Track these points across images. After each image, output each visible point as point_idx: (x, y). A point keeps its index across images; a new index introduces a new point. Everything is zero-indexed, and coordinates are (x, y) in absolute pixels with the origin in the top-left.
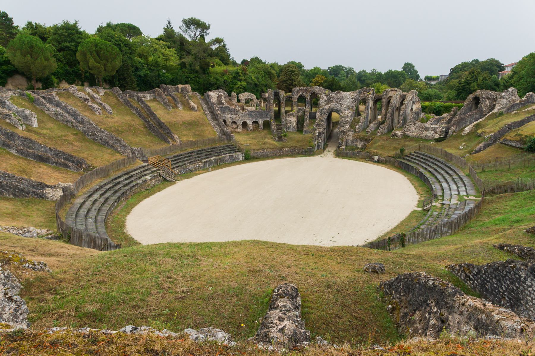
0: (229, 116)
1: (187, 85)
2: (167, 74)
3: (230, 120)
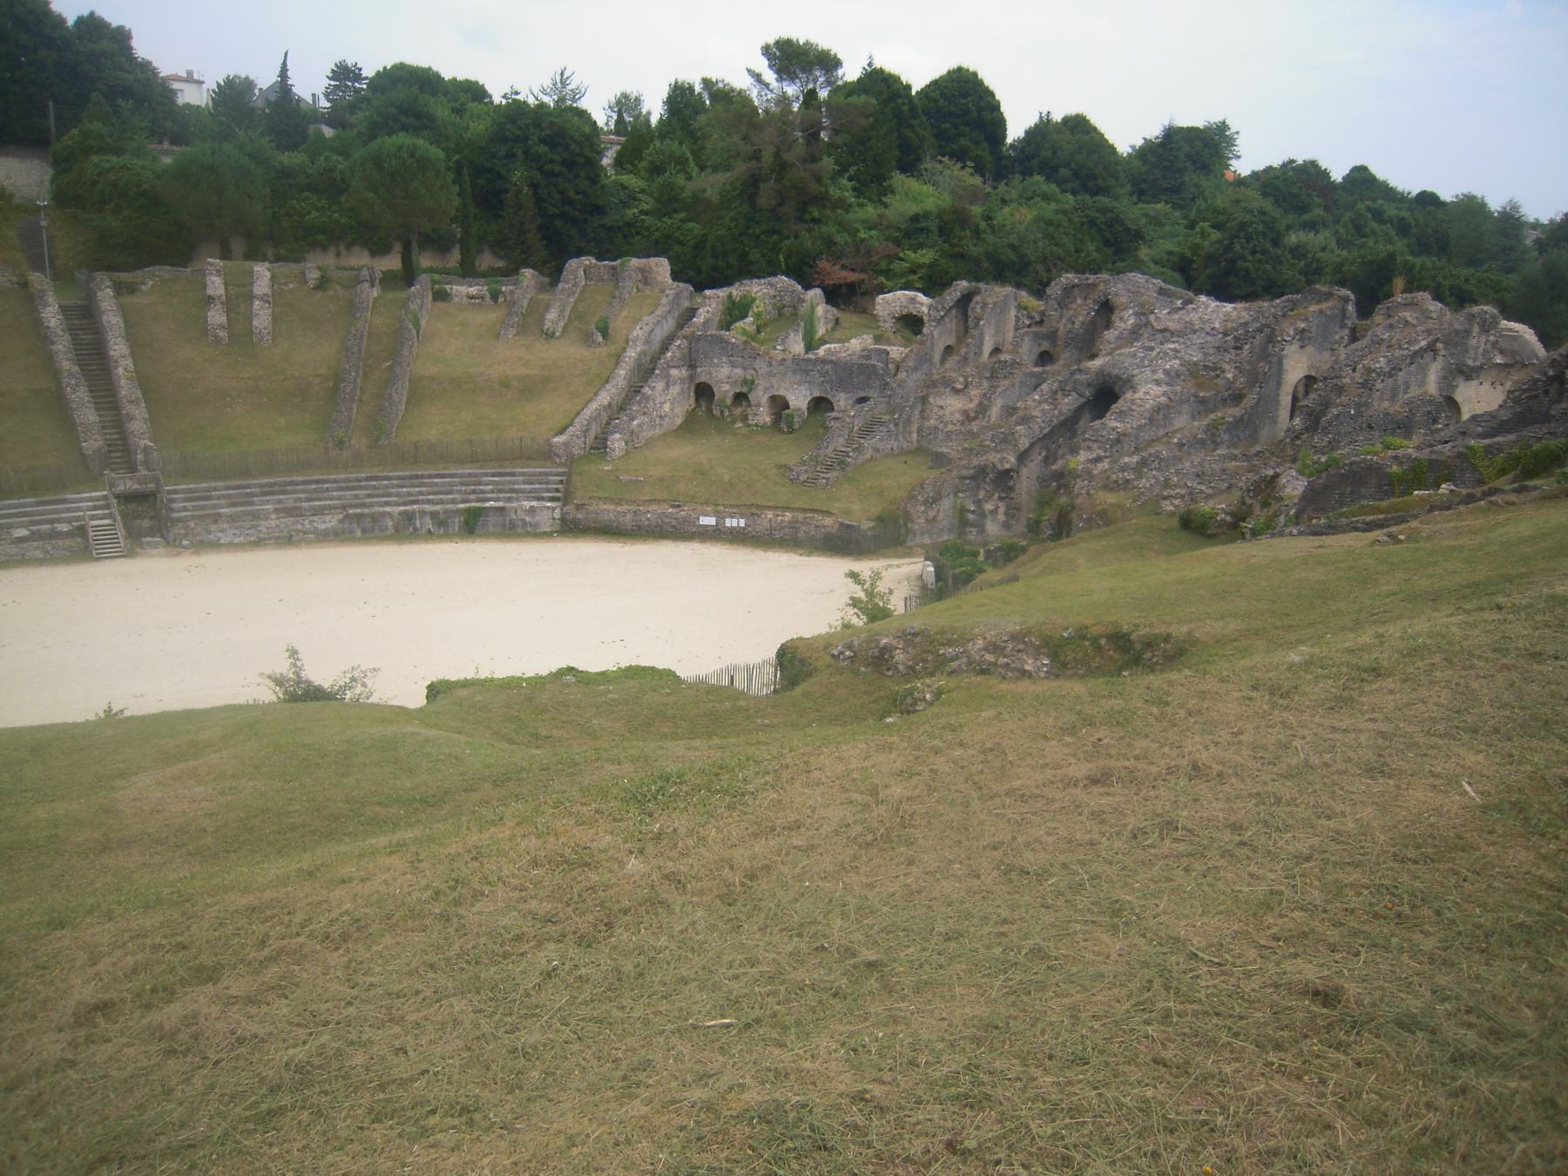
0: (725, 371)
1: (653, 261)
2: (691, 225)
3: (727, 387)
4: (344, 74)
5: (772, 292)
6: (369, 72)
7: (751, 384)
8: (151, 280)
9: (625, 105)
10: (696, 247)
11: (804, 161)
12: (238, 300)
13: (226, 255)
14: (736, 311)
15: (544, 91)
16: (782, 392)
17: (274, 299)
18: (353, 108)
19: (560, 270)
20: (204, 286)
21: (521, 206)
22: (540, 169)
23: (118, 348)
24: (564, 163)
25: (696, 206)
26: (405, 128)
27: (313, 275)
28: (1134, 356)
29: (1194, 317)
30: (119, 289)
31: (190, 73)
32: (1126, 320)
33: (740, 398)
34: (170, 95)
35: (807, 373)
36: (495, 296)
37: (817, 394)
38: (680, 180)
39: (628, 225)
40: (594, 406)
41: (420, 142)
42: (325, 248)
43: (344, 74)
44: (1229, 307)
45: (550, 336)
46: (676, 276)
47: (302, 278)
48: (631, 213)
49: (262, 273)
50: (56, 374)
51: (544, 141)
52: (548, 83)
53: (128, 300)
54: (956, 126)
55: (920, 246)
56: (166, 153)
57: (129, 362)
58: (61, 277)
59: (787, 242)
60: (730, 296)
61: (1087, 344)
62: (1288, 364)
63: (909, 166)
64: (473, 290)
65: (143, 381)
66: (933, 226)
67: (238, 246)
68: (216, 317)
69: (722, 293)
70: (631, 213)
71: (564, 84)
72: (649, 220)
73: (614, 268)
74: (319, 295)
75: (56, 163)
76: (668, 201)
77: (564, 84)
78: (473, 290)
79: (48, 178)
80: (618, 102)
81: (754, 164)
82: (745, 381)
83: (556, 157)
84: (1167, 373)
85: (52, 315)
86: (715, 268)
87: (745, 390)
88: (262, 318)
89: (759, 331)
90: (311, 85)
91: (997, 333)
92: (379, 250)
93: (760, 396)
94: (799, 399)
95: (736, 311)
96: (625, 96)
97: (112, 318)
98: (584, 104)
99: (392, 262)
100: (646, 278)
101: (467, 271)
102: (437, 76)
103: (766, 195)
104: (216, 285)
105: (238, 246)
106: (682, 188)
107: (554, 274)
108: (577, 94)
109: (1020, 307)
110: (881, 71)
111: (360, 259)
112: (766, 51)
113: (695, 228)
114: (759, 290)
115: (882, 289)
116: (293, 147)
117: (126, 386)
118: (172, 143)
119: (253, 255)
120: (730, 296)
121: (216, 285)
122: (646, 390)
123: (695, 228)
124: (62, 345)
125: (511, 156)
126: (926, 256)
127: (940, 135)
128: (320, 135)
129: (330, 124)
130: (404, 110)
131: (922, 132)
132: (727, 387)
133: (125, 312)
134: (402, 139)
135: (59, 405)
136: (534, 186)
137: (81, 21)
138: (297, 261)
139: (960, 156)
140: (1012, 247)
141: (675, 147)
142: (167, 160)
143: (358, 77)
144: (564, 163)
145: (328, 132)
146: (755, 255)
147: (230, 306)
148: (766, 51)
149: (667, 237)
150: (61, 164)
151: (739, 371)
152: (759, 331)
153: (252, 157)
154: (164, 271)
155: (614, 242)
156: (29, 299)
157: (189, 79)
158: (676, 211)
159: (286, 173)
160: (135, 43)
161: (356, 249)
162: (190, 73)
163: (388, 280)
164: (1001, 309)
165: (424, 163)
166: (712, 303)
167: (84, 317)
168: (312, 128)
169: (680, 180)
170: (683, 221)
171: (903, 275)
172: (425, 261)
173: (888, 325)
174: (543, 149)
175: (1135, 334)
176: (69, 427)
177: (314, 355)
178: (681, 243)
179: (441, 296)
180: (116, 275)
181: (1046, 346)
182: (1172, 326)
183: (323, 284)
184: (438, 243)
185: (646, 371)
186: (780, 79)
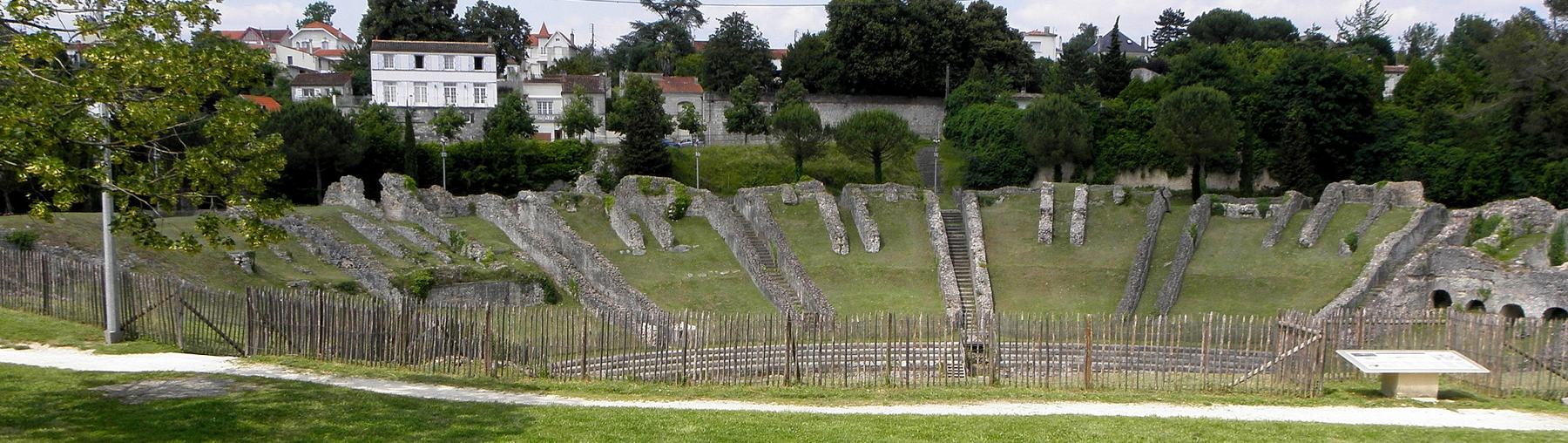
0: (1462, 281)
3: (1464, 295)
5: (1521, 212)
6: (1191, 16)
7: (1487, 293)
8: (1005, 199)
9: (1417, 35)
12: (1059, 214)
14: (1479, 228)
15: (1348, 22)
17: (1086, 214)
19: (1320, 192)
21: (1295, 137)
22: (1316, 106)
23: (976, 244)
24: (1338, 100)
25: (1467, 133)
26: (1204, 77)
27: (1119, 194)
30: (980, 201)
31: (1047, 29)
33: (1476, 305)
34: (1028, 51)
35: (1544, 285)
36: (1263, 213)
37: (1553, 305)
38: (1449, 109)
39: (1396, 150)
40: (1333, 305)
41: (1211, 89)
42: (1133, 171)
45: (1306, 247)
46: (1427, 197)
47: (1110, 195)
48: (1398, 140)
49: (1081, 191)
50: (935, 260)
52: (1352, 14)
53: (987, 210)
57: (983, 254)
59: (1552, 164)
60: (1480, 215)
64: (1245, 207)
65: (988, 265)
67: (1068, 170)
68: (1045, 224)
70: (1398, 140)
72: (1416, 144)
73: (1370, 190)
74: (1123, 208)
76: (1438, 128)
77: (1368, 14)
78: (1245, 207)
79: (941, 118)
80: (1413, 32)
82: (1482, 291)
83: (1331, 95)
85: (936, 221)
86: (1475, 188)
87: (1481, 298)
88: (1077, 228)
92: (1175, 173)
93: (1496, 304)
96: (1419, 28)
97: (974, 224)
98: (1385, 32)
99: (1183, 184)
100: (1400, 197)
102: (1248, 17)
103: (1534, 121)
104: (1047, 201)
105: (1068, 170)
106: (1449, 117)
111: (1161, 180)
113: (1460, 152)
116: (1114, 94)
117: (979, 272)
119: (1076, 178)
120: (1480, 215)
121: (1047, 201)
122: (1383, 295)
123: (1460, 152)
124: (941, 241)
125: (1289, 96)
129: (1150, 67)
130: (1204, 63)
132: (1464, 295)
133: (982, 218)
134: (1199, 88)
135: (932, 277)
136: (1306, 119)
138: (1108, 183)
142: (1023, 106)
143: (1181, 21)
144: (1338, 100)
145: (1147, 75)
146: (1517, 177)
147: (1055, 215)
149: (1433, 160)
150: (952, 110)
151: (1476, 281)
152: (1503, 247)
153: (1082, 104)
155: (1375, 168)
156: (924, 209)
157: (1047, 34)
158: (1442, 137)
159: (1108, 114)
160: (1007, 18)
161: (1157, 173)
162: (1047, 29)
165: (1213, 105)
166: (1459, 219)
167: (954, 222)
168: (1134, 74)
169: (1449, 109)
170: (1448, 146)
172: (1212, 181)
174: (1320, 89)
176: (937, 291)
178: (1445, 166)
179: (1218, 211)
180: (981, 192)
183: (1126, 200)
184: (1225, 168)
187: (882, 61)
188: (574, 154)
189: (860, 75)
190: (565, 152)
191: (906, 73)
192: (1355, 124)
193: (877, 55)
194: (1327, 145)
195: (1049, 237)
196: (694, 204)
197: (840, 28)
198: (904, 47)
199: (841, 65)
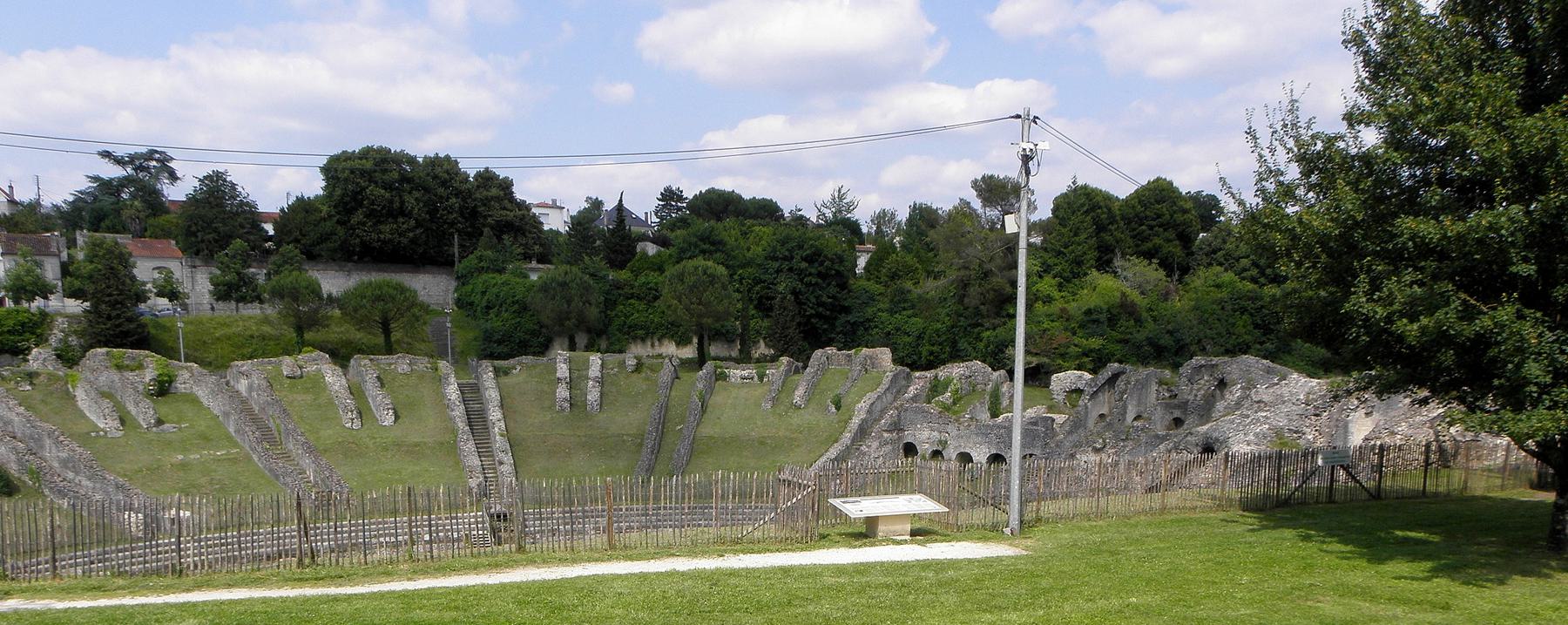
0: (926, 434)
4: (670, 196)
6: (689, 194)
7: (944, 443)
8: (522, 369)
9: (882, 218)
10: (919, 337)
11: (1001, 269)
12: (575, 382)
13: (572, 347)
14: (936, 388)
16: (967, 450)
18: (673, 226)
20: (555, 370)
23: (495, 415)
24: (820, 275)
25: (921, 306)
26: (703, 252)
27: (631, 362)
28: (1232, 422)
29: (1285, 391)
30: (497, 371)
31: (554, 201)
32: (1235, 392)
33: (937, 454)
36: (761, 378)
39: (869, 320)
42: (643, 340)
43: (670, 196)
44: (1315, 381)
46: (894, 361)
47: (622, 364)
48: (870, 311)
49: (595, 360)
50: (454, 431)
51: (805, 259)
53: (504, 380)
54: (1151, 228)
55: (1092, 335)
56: (533, 270)
57: (502, 424)
58: (459, 361)
61: (1205, 411)
62: (1353, 428)
63: (1104, 265)
64: (746, 373)
66: (1103, 317)
67: (582, 339)
69: (929, 374)
71: (841, 198)
74: (635, 375)
75: (458, 278)
78: (746, 373)
79: (452, 288)
80: (879, 216)
81: (962, 273)
84: (1256, 435)
85: (452, 391)
88: (593, 395)
89: (954, 403)
90: (643, 206)
91: (1139, 404)
92: (682, 342)
93: (951, 453)
94: (980, 455)
95: (936, 388)
97: (492, 394)
99: (689, 352)
101: (744, 358)
104: (563, 370)
105: (582, 339)
107: (803, 357)
108: (850, 207)
109: (1160, 383)
110: (1085, 187)
112: (975, 184)
113: (917, 323)
114: (955, 371)
115: (1060, 369)
117: (499, 442)
118: (539, 262)
119: (590, 347)
121: (563, 370)
122: (864, 448)
124: (459, 412)
126: (1095, 343)
127: (1140, 238)
128: (645, 254)
131: (1119, 235)
134: (700, 262)
135: (451, 449)
136: (795, 293)
137: (479, 175)
138: (621, 352)
139: (1149, 255)
140: (1170, 333)
141: (910, 259)
142: (534, 277)
143: (680, 198)
145: (652, 249)
146: (963, 344)
147: (571, 384)
148: (975, 184)
149: (898, 329)
150: (462, 279)
151: (936, 433)
152: (954, 403)
153: (592, 275)
154: (527, 359)
156: (441, 381)
157: (554, 206)
159: (618, 286)
160: (514, 189)
161: (666, 342)
162: (554, 201)
163: (685, 364)
164: (1143, 385)
165: (713, 278)
166: (920, 381)
168: (640, 246)
169: (909, 285)
171: (1077, 357)
173: (1061, 398)
174: (804, 265)
175: (1238, 405)
177: (632, 418)
181: (1177, 414)
182: (1266, 398)
183: (639, 367)
184: (724, 336)
185: (863, 432)
186: (984, 206)
187: (386, 228)
188: (23, 325)
189: (363, 243)
190: (11, 323)
191: (413, 241)
192: (833, 297)
193: (379, 222)
194: (811, 316)
195: (567, 405)
196: (180, 379)
197: (338, 192)
198: (409, 215)
199: (341, 231)
